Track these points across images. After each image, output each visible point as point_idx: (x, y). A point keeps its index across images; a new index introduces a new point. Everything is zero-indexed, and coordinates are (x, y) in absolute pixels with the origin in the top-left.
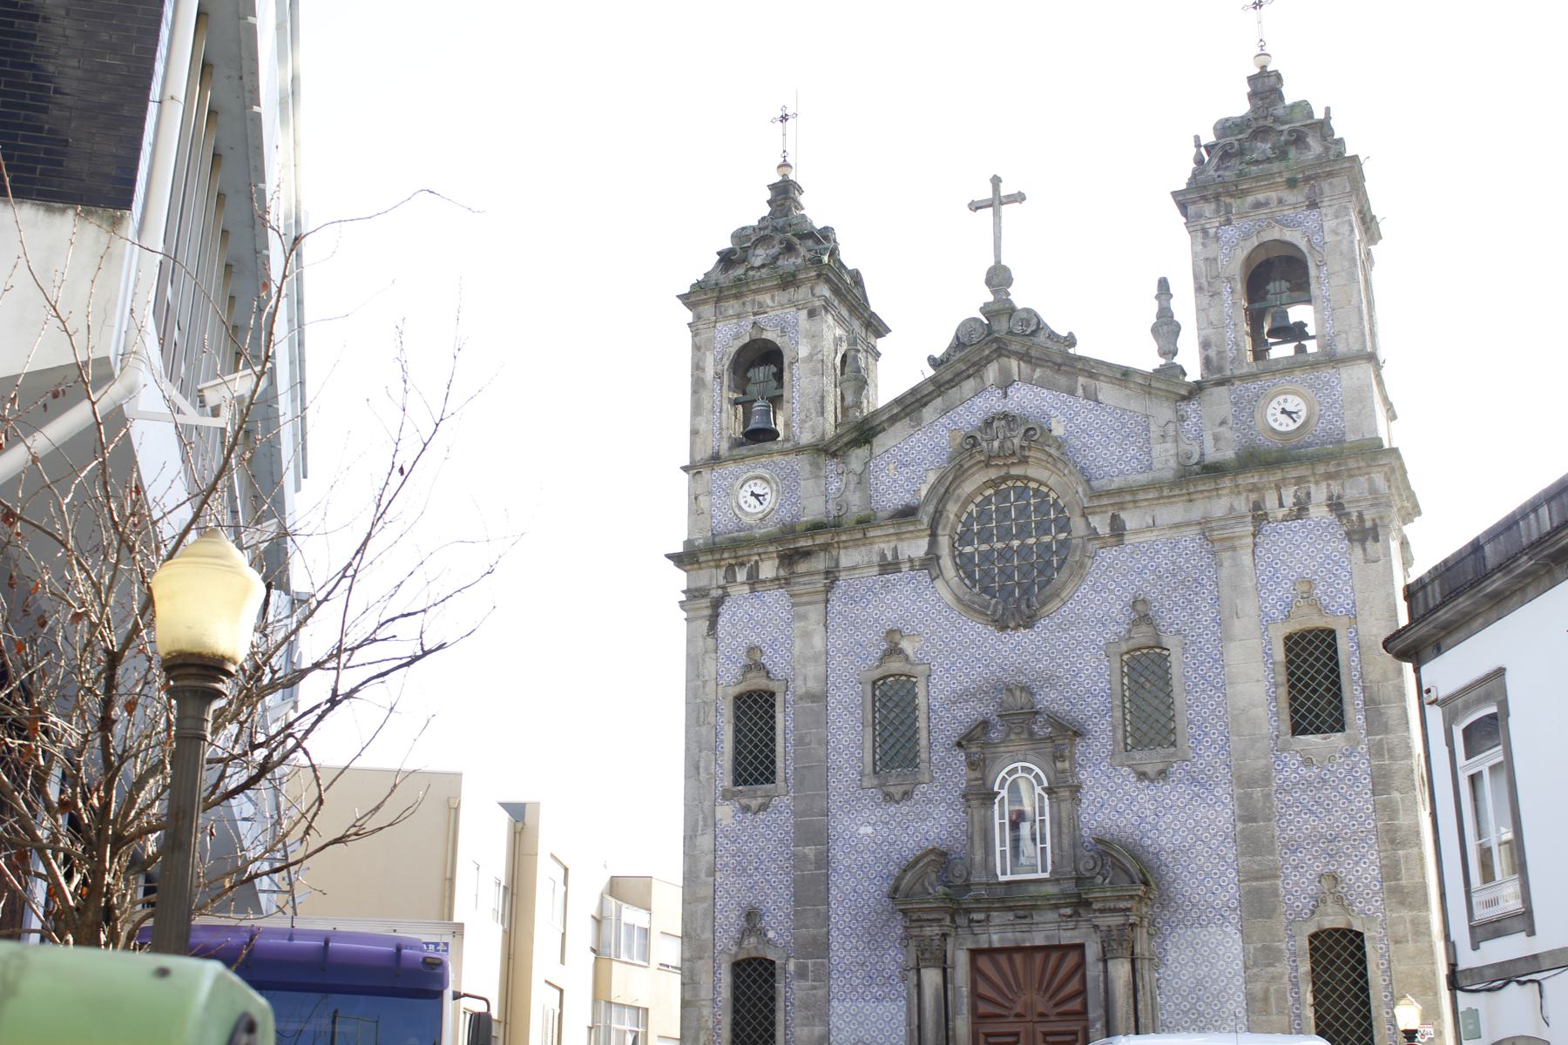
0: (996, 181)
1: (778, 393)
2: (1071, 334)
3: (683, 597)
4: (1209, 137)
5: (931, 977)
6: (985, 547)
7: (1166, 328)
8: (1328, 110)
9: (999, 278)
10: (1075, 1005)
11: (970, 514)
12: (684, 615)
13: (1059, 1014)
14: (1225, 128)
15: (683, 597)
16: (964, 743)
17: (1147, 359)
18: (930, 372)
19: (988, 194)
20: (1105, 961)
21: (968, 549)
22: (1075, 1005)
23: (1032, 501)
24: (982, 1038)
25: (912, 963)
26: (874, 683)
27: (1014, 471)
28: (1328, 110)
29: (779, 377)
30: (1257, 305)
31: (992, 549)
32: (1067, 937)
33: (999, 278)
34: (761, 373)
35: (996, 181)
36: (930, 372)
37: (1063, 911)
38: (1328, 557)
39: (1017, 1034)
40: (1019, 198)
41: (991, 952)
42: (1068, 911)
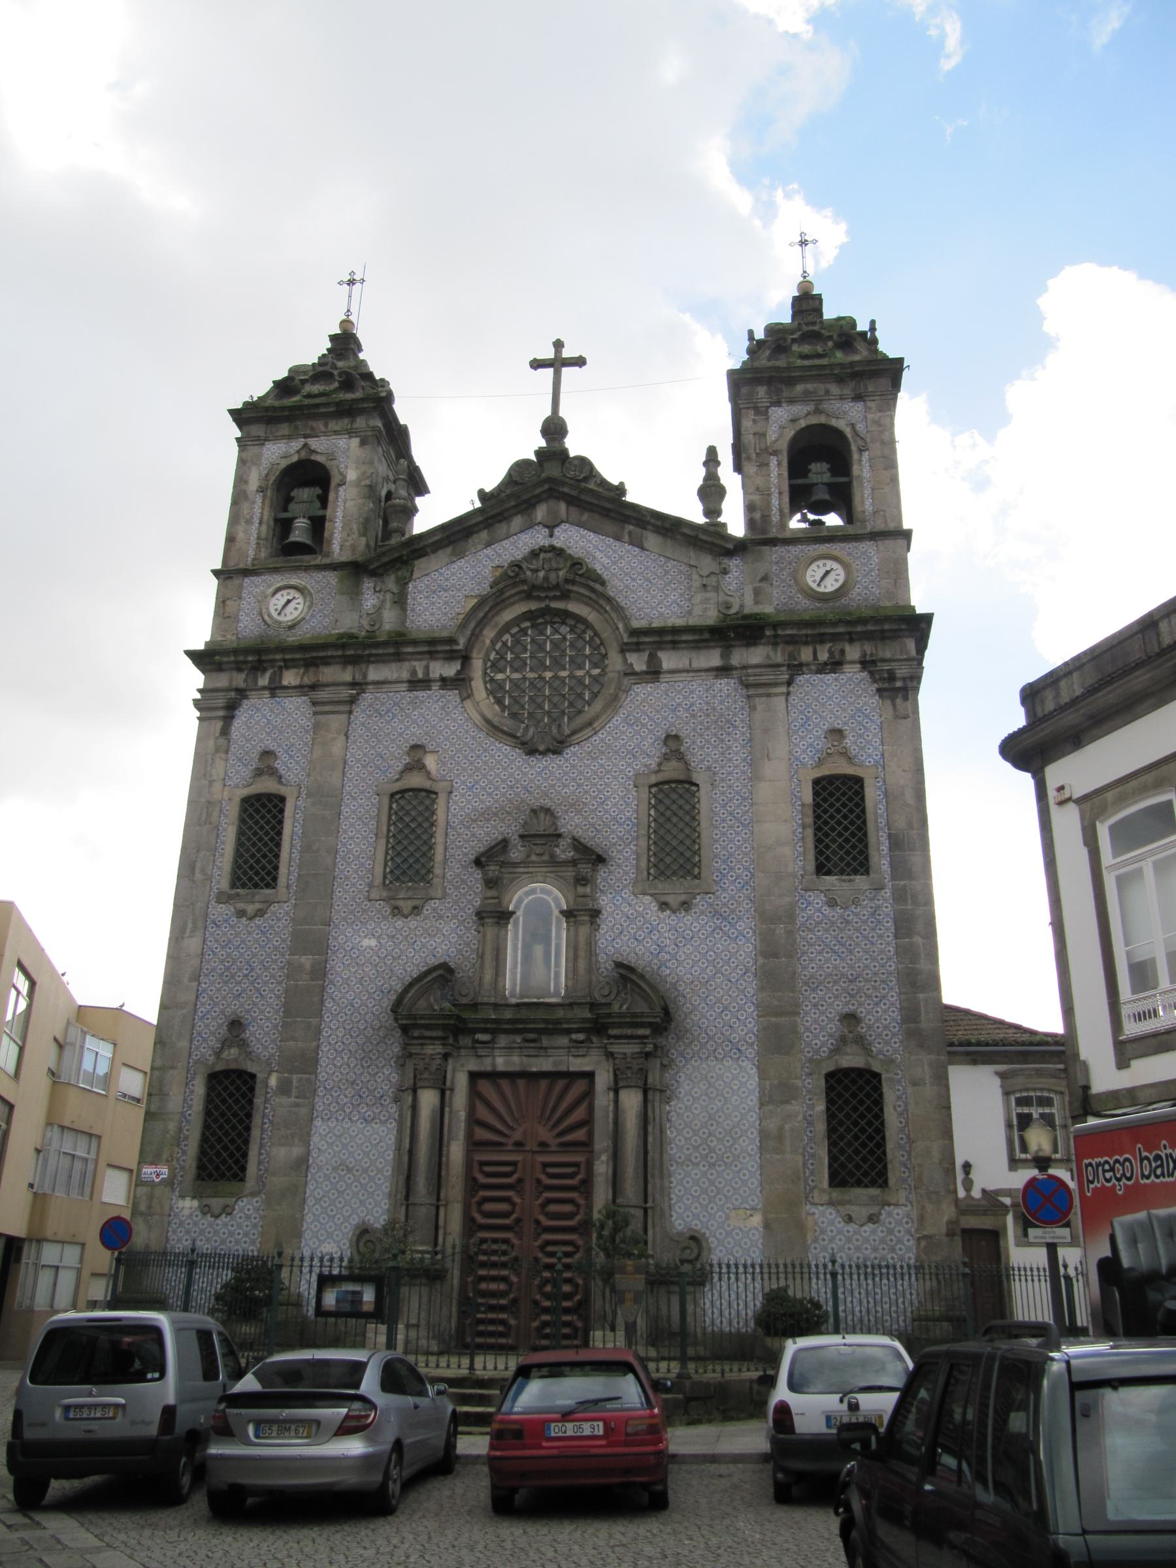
0: (558, 345)
1: (320, 513)
2: (622, 484)
3: (198, 696)
4: (760, 335)
5: (428, 1099)
6: (516, 676)
7: (711, 492)
8: (873, 323)
9: (554, 429)
10: (579, 1135)
11: (505, 644)
12: (198, 714)
13: (562, 1144)
14: (772, 330)
15: (198, 696)
16: (483, 859)
17: (694, 513)
18: (478, 505)
19: (550, 354)
20: (617, 1092)
21: (500, 676)
22: (579, 1135)
23: (568, 637)
24: (476, 1167)
25: (409, 1083)
26: (392, 795)
27: (555, 605)
28: (873, 323)
29: (324, 501)
30: (799, 481)
31: (524, 678)
32: (577, 1064)
33: (554, 429)
34: (305, 494)
35: (558, 345)
36: (478, 505)
37: (574, 1036)
38: (859, 710)
39: (514, 1164)
40: (580, 362)
41: (493, 1076)
42: (581, 1037)
